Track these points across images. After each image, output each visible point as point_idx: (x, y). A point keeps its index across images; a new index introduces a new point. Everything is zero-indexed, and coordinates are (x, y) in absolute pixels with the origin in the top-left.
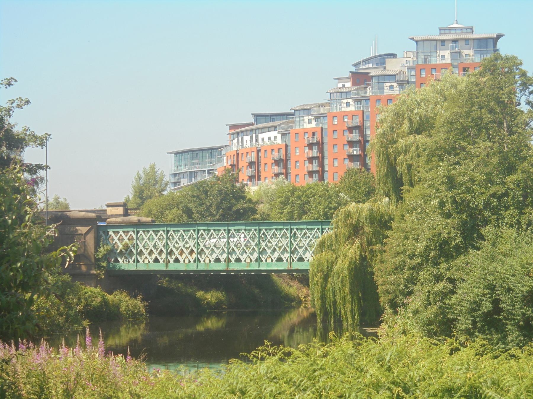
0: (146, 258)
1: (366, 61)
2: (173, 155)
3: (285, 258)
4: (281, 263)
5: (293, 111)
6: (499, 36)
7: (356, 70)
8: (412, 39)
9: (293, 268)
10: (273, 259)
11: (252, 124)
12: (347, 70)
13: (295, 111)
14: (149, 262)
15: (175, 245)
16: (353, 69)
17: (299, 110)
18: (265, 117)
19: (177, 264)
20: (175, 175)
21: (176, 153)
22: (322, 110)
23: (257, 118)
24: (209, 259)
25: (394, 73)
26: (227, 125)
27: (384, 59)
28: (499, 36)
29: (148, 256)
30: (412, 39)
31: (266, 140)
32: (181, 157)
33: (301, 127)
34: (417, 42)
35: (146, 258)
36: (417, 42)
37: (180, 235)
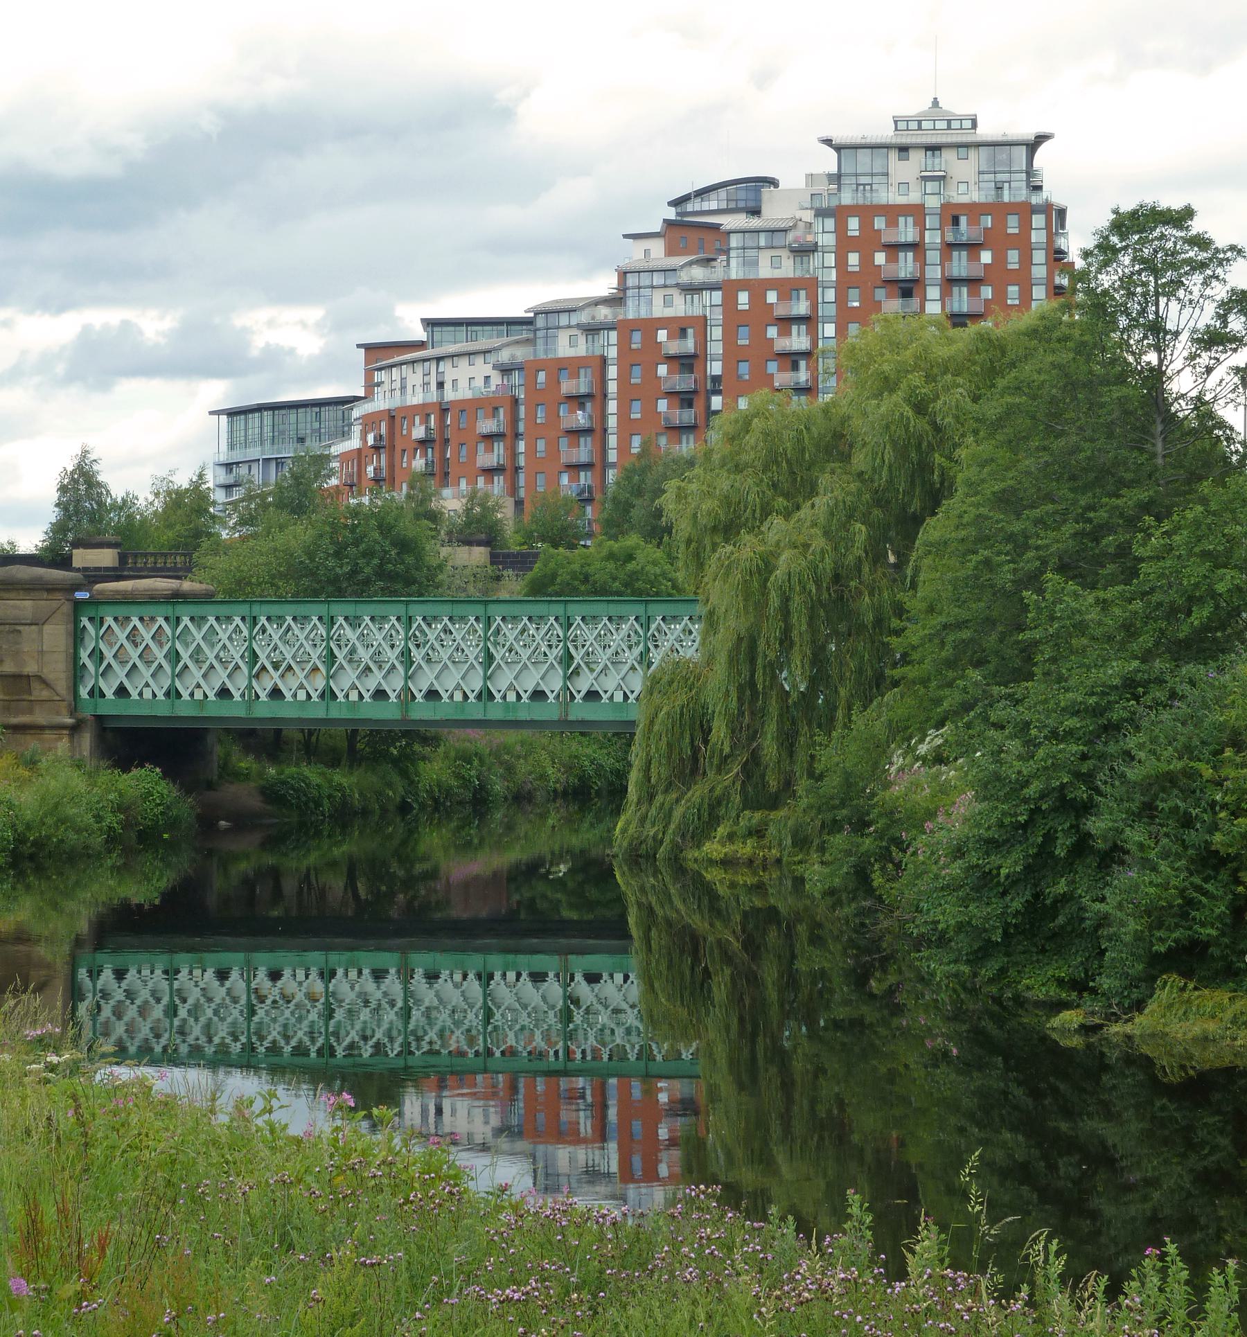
0: (147, 685)
1: (702, 193)
2: (224, 418)
3: (606, 692)
4: (383, 703)
5: (532, 315)
6: (1041, 139)
7: (678, 214)
8: (828, 142)
9: (571, 718)
10: (522, 693)
11: (421, 345)
12: (658, 215)
13: (536, 314)
14: (154, 695)
15: (222, 654)
16: (671, 214)
17: (547, 313)
18: (452, 328)
19: (381, 703)
20: (229, 466)
21: (232, 413)
22: (604, 313)
23: (436, 329)
24: (518, 693)
25: (783, 225)
26: (359, 346)
27: (758, 191)
28: (1041, 139)
29: (151, 682)
30: (828, 142)
31: (463, 383)
32: (243, 422)
33: (550, 356)
34: (839, 149)
35: (198, 686)
36: (839, 149)
37: (235, 631)
